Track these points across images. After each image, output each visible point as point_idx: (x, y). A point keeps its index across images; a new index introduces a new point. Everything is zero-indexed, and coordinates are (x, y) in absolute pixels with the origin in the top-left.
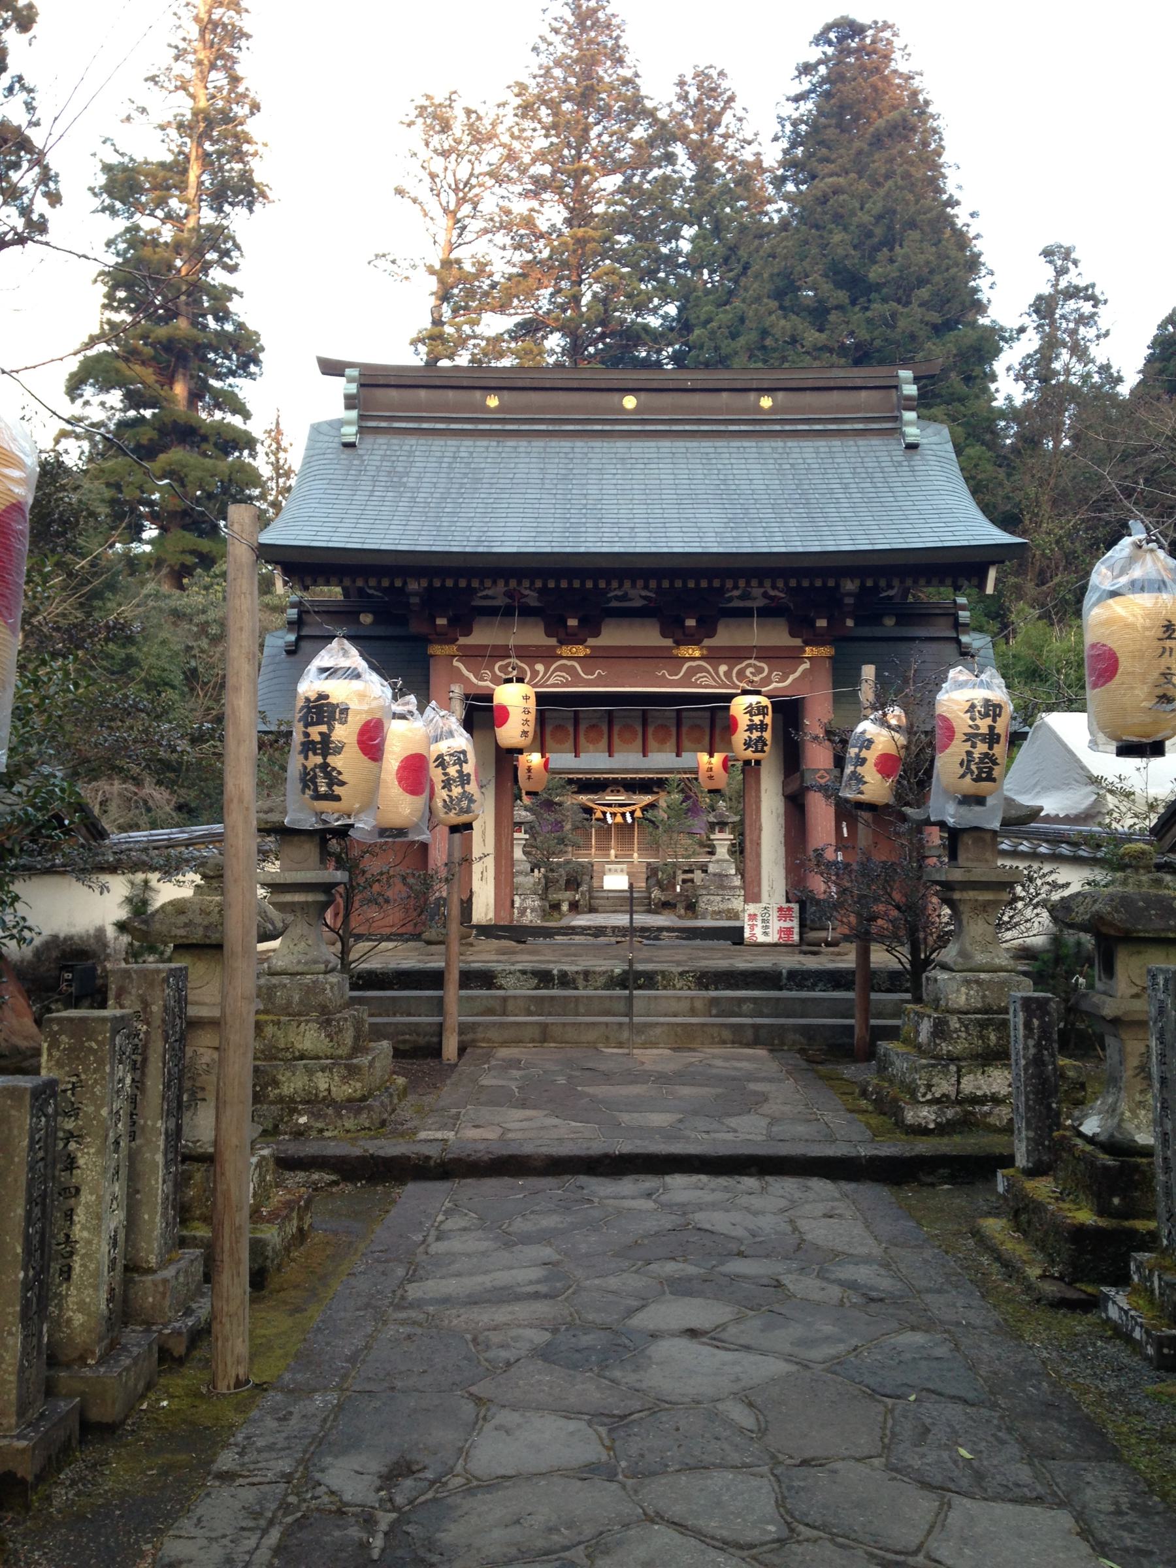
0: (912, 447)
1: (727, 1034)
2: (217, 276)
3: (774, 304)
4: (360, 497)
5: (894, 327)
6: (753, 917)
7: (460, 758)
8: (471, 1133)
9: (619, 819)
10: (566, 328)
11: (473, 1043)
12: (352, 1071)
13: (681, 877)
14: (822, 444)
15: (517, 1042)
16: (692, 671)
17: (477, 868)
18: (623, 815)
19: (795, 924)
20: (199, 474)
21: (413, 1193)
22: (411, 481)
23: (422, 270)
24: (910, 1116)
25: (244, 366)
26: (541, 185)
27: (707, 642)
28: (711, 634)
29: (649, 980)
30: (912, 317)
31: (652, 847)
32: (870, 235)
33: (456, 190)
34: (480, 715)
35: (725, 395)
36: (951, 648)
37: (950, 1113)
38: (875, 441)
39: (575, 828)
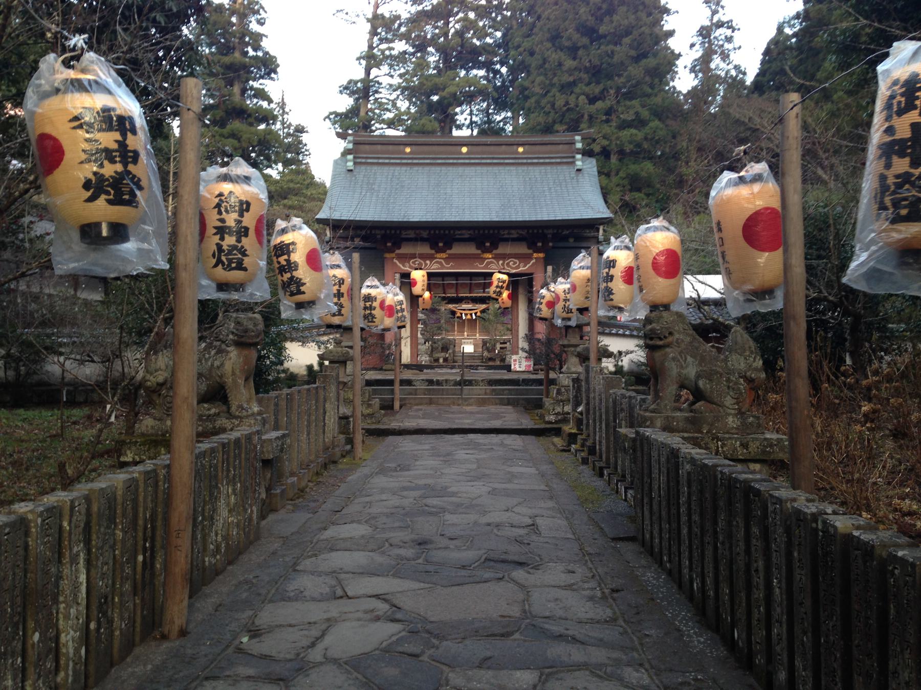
0: (579, 170)
1: (497, 401)
2: (254, 27)
3: (549, 45)
4: (357, 195)
5: (612, 58)
6: (515, 361)
7: (401, 303)
8: (407, 424)
9: (469, 317)
10: (441, 50)
11: (405, 404)
12: (369, 406)
13: (498, 346)
14: (542, 168)
15: (421, 404)
16: (489, 263)
17: (403, 342)
18: (471, 315)
19: (532, 363)
20: (248, 136)
22: (376, 187)
23: (362, 17)
24: (547, 419)
25: (269, 74)
27: (495, 252)
28: (496, 248)
29: (470, 383)
30: (622, 51)
31: (485, 330)
32: (600, 8)
34: (406, 282)
35: (503, 147)
37: (560, 417)
38: (565, 167)
39: (446, 322)
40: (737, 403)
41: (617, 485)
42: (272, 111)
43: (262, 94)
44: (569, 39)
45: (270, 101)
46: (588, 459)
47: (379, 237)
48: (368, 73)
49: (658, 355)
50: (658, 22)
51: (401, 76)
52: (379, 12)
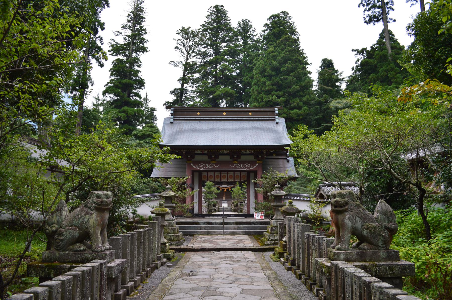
0: (277, 123)
2: (136, 68)
16: (236, 166)
21: (188, 254)
22: (183, 130)
26: (207, 45)
33: (189, 47)
36: (285, 161)
37: (273, 242)
40: (384, 244)
41: (311, 287)
42: (141, 102)
43: (137, 95)
44: (268, 72)
45: (140, 98)
46: (291, 268)
47: (184, 153)
48: (182, 85)
49: (340, 217)
50: (305, 68)
51: (196, 87)
52: (188, 61)
